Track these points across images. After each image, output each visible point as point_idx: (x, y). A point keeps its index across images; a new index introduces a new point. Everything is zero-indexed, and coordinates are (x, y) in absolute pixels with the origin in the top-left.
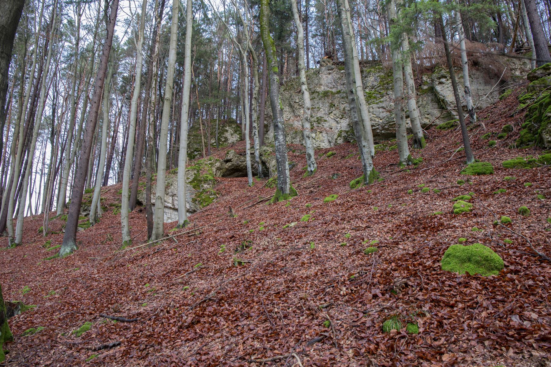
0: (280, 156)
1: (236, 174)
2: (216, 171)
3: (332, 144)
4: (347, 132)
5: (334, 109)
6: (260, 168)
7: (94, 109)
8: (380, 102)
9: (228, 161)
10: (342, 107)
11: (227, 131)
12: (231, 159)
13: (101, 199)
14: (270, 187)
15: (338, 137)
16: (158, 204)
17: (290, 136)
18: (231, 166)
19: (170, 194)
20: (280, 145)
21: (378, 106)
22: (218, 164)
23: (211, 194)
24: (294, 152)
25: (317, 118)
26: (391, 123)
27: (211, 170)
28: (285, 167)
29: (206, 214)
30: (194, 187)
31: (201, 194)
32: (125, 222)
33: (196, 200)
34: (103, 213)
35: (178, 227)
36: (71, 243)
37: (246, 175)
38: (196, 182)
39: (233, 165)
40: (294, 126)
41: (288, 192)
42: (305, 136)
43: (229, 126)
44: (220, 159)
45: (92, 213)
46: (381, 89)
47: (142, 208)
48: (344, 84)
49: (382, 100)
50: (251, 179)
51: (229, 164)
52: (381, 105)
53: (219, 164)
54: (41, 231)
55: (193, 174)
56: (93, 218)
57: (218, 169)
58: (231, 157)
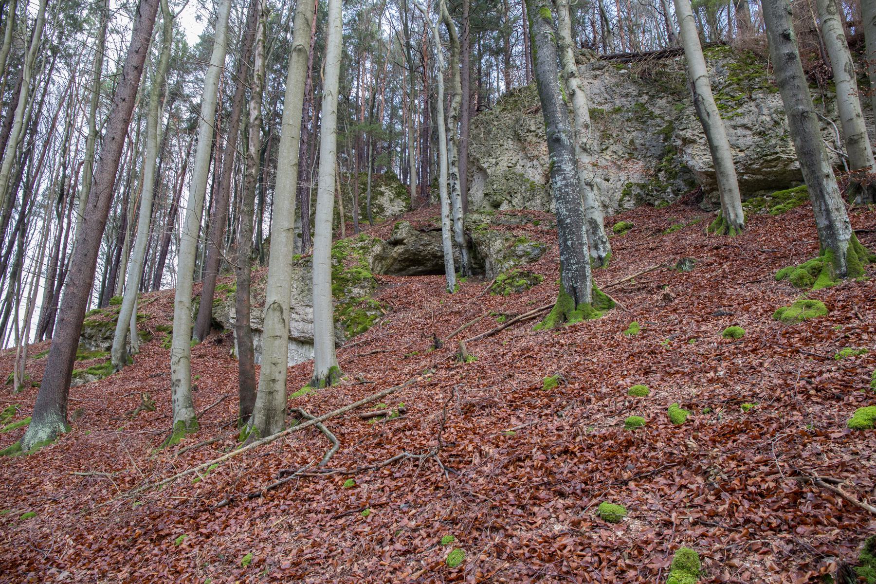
2: (374, 262)
3: (610, 210)
4: (643, 187)
5: (611, 141)
6: (465, 258)
7: (121, 115)
8: (737, 115)
9: (397, 243)
10: (628, 137)
11: (382, 194)
12: (403, 240)
13: (139, 318)
14: (500, 293)
15: (625, 195)
16: (272, 324)
17: (519, 196)
18: (402, 253)
20: (566, 186)
21: (733, 123)
22: (377, 249)
23: (370, 308)
24: (536, 224)
26: (769, 158)
27: (365, 259)
28: (580, 237)
29: (368, 350)
32: (180, 372)
34: (143, 345)
35: (315, 383)
36: (52, 416)
37: (440, 270)
40: (526, 176)
41: (589, 299)
42: (583, 183)
43: (386, 185)
45: (116, 343)
46: (734, 90)
47: (223, 335)
48: (627, 95)
49: (740, 110)
50: (451, 277)
51: (399, 249)
52: (739, 121)
54: (11, 381)
56: (119, 355)
57: (379, 258)
58: (404, 235)
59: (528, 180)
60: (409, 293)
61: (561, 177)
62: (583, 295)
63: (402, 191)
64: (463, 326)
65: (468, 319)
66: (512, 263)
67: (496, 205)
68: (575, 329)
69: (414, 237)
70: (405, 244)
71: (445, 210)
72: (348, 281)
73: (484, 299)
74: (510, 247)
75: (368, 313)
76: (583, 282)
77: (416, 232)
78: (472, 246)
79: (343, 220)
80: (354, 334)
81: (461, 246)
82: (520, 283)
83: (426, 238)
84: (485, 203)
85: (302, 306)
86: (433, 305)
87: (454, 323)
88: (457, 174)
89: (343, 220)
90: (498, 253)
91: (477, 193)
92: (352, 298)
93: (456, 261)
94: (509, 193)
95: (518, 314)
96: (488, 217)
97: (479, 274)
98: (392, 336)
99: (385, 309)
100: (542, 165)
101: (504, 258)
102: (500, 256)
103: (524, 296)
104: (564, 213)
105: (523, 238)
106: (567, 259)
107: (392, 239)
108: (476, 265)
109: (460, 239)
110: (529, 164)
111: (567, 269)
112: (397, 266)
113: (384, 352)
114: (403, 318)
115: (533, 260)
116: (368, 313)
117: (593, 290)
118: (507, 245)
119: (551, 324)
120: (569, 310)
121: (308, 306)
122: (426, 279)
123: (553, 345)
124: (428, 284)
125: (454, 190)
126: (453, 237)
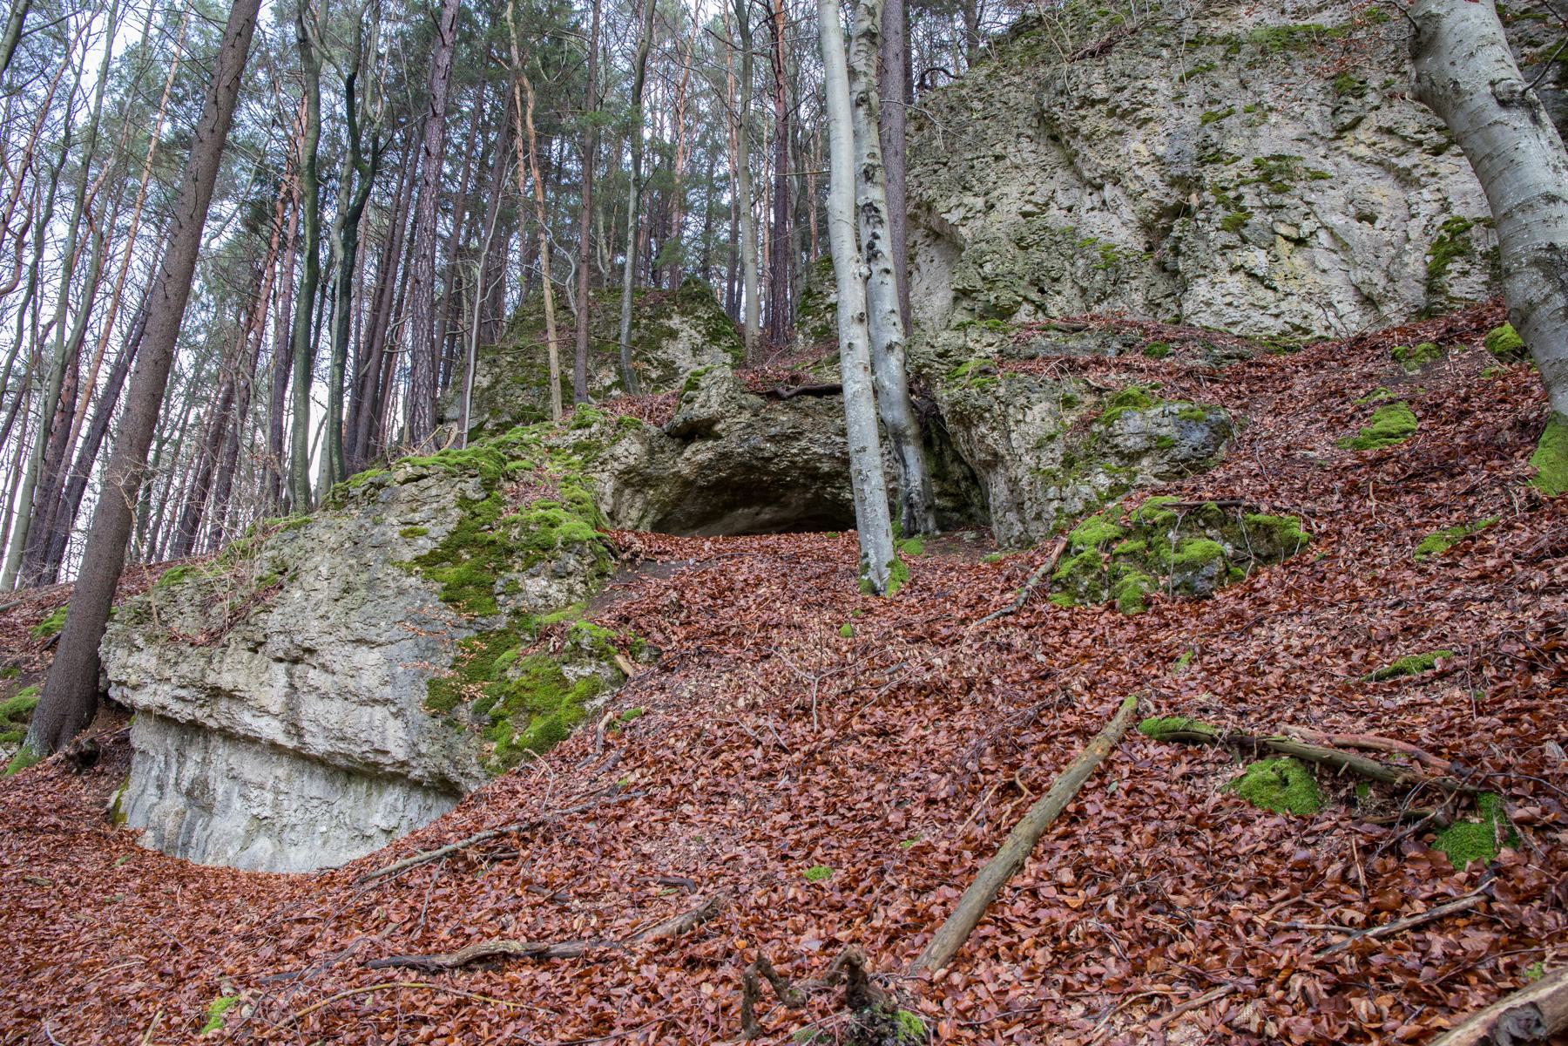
1: (742, 515)
2: (618, 492)
3: (1388, 309)
6: (915, 471)
11: (673, 334)
12: (712, 422)
19: (278, 644)
22: (630, 450)
25: (1258, 165)
31: (497, 649)
37: (837, 517)
39: (724, 456)
40: (1084, 232)
43: (683, 313)
44: (646, 423)
50: (877, 536)
51: (701, 452)
55: (450, 499)
57: (633, 480)
58: (715, 408)
59: (1093, 243)
60: (722, 594)
69: (746, 416)
70: (718, 437)
74: (1085, 424)
75: (569, 672)
77: (753, 399)
83: (784, 419)
85: (344, 642)
88: (881, 207)
90: (1039, 446)
92: (517, 613)
94: (1036, 283)
96: (988, 338)
97: (959, 526)
100: (1134, 197)
101: (1069, 463)
102: (1050, 460)
107: (678, 419)
108: (955, 490)
109: (898, 415)
116: (569, 672)
118: (1071, 418)
121: (360, 641)
122: (786, 544)
124: (794, 559)
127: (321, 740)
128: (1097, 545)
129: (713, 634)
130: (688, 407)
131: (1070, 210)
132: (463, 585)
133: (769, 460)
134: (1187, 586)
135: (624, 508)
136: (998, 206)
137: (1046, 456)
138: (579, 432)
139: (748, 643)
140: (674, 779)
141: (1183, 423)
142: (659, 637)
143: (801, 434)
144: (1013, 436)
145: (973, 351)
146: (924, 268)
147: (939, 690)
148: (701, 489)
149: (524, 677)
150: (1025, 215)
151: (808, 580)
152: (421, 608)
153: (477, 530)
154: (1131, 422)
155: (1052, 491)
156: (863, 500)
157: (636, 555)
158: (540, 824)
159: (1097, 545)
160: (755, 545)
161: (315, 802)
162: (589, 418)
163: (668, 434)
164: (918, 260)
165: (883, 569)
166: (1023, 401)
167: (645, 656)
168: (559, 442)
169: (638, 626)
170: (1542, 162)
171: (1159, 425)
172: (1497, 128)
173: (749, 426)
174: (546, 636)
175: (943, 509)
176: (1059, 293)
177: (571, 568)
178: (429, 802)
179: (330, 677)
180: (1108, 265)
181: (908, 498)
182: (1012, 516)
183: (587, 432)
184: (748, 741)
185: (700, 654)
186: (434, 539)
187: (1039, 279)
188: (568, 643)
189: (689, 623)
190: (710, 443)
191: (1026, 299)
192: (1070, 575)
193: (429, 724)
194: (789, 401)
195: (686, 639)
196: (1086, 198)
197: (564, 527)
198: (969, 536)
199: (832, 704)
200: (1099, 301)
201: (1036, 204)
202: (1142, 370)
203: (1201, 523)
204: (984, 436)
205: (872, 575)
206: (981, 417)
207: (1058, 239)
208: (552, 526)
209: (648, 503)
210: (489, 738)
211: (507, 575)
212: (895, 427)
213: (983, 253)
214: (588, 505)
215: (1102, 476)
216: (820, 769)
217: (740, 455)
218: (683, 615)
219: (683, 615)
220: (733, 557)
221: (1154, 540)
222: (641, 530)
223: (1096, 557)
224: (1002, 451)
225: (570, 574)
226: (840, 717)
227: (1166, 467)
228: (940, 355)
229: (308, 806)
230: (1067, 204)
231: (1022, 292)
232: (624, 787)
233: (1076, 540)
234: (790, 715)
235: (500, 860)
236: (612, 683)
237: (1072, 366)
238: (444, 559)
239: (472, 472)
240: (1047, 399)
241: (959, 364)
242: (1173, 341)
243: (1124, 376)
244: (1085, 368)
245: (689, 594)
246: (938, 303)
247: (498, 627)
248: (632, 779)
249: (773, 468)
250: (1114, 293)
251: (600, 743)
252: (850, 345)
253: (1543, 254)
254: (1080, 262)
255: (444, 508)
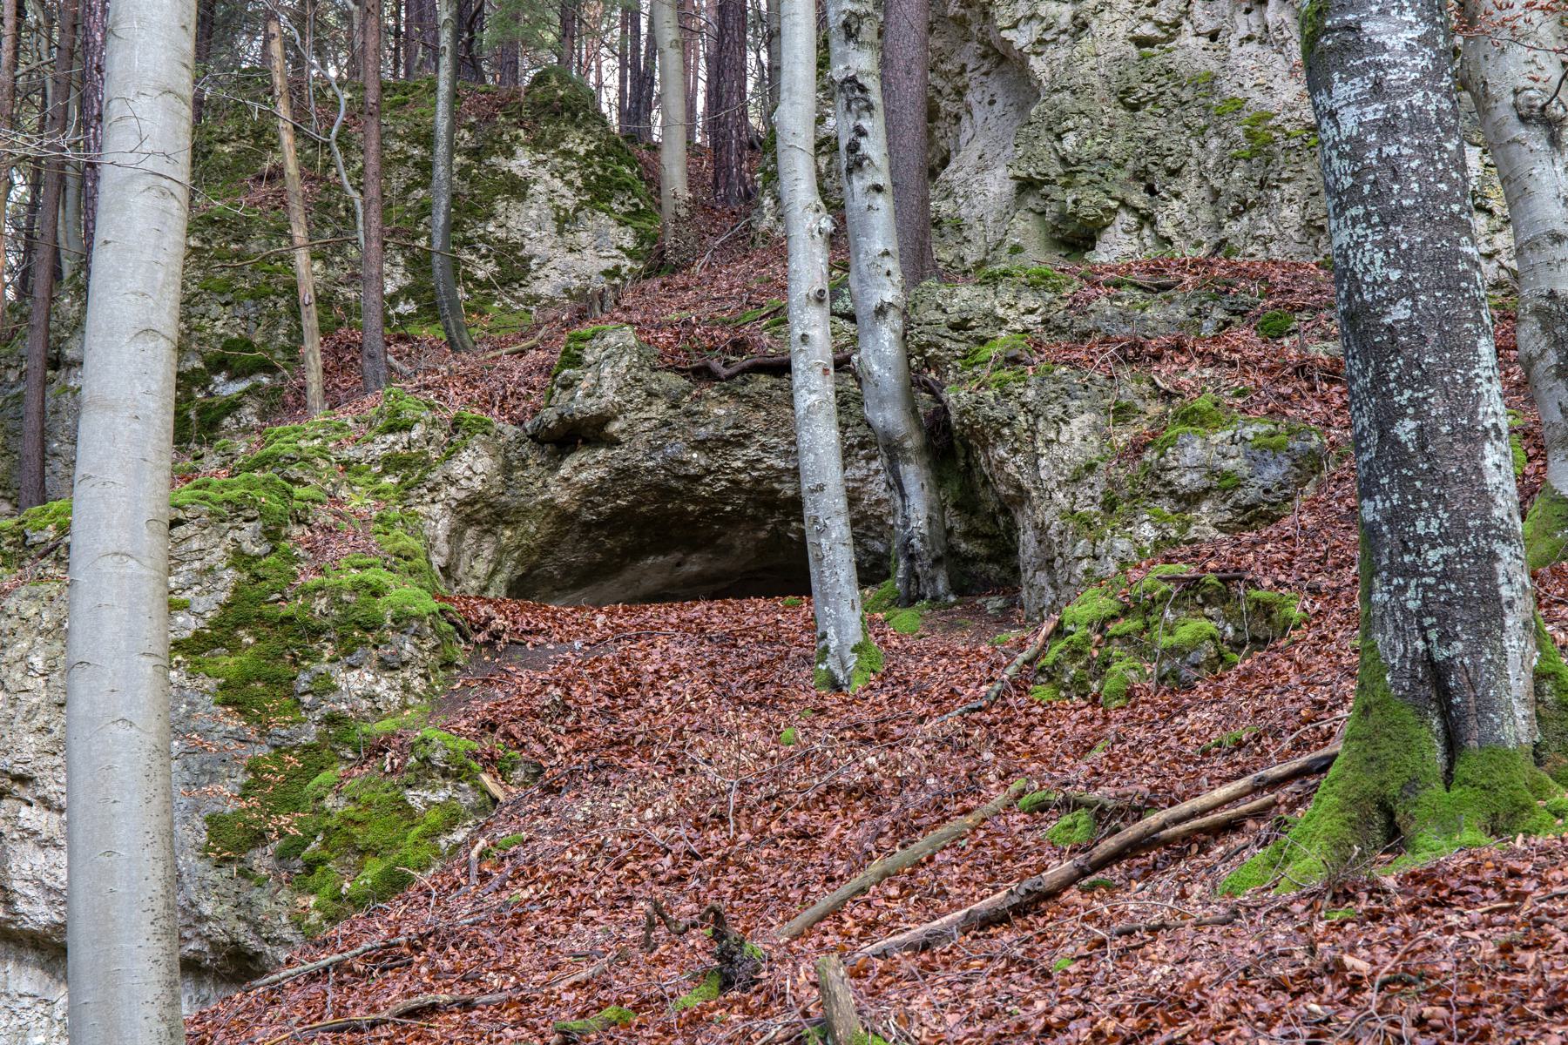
0: (1403, 260)
2: (455, 535)
6: (917, 506)
9: (569, 436)
11: (517, 189)
12: (603, 419)
14: (1080, 685)
20: (1387, 128)
22: (474, 467)
24: (1274, 331)
28: (1465, 399)
29: (394, 995)
30: (234, 697)
33: (259, 838)
37: (787, 572)
38: (254, 645)
39: (624, 474)
40: (1228, 87)
41: (1517, 725)
42: (1504, 111)
43: (536, 144)
50: (840, 606)
51: (586, 468)
53: (484, 464)
57: (480, 514)
58: (610, 396)
59: (1238, 106)
60: (623, 691)
61: (1359, 85)
62: (1486, 706)
63: (619, 172)
64: (876, 866)
65: (905, 831)
66: (1147, 531)
67: (1077, 238)
68: (1432, 892)
69: (659, 408)
70: (613, 442)
71: (808, 266)
72: (316, 633)
73: (1001, 719)
74: (1138, 448)
75: (415, 797)
76: (1482, 636)
78: (950, 447)
79: (310, 320)
80: (340, 907)
81: (893, 450)
82: (1184, 634)
83: (720, 411)
84: (1024, 229)
86: (734, 752)
87: (840, 849)
89: (310, 320)
90: (1076, 479)
91: (982, 184)
92: (332, 720)
93: (865, 524)
94: (1141, 176)
95: (1151, 805)
96: (1028, 300)
97: (988, 586)
98: (519, 921)
99: (503, 773)
101: (1110, 506)
103: (1199, 705)
104: (1378, 272)
105: (1203, 403)
106: (1395, 517)
107: (550, 415)
108: (976, 553)
109: (889, 416)
110: (1244, 24)
111: (1394, 570)
112: (573, 554)
113: (467, 1006)
114: (590, 823)
115: (1254, 516)
116: (415, 797)
117: (1540, 677)
118: (1123, 437)
119: (1310, 863)
120: (1412, 785)
122: (717, 616)
123: (1305, 984)
124: (728, 641)
125: (858, 164)
126: (845, 402)
127: (44, 908)
128: (1090, 625)
129: (612, 744)
130: (566, 395)
131: (1213, 36)
132: (249, 681)
133: (697, 479)
134: (1174, 674)
135: (465, 558)
136: (1094, 24)
137: (1083, 492)
138: (391, 438)
139: (658, 754)
140: (574, 891)
141: (1257, 454)
142: (538, 749)
143: (747, 436)
144: (1043, 462)
145: (1005, 322)
146: (978, 114)
147: (870, 791)
148: (588, 525)
149: (352, 807)
150: (1141, 42)
151: (744, 672)
152: (188, 716)
153: (263, 599)
154: (1188, 451)
155: (1082, 546)
156: (820, 560)
157: (496, 635)
158: (430, 935)
159: (1090, 625)
160: (673, 619)
161: (27, 1002)
162: (408, 415)
163: (533, 437)
164: (970, 97)
165: (847, 654)
166: (1057, 410)
167: (519, 774)
168: (359, 454)
169: (508, 735)
170: (1553, 192)
171: (1224, 456)
172: (1514, 148)
173: (666, 424)
174: (378, 750)
175: (974, 559)
176: (1177, 196)
177: (406, 656)
178: (205, 992)
179: (56, 816)
180: (1255, 152)
181: (907, 545)
182: (1042, 578)
183: (405, 437)
184: (657, 850)
185: (596, 769)
186: (199, 615)
187: (1146, 169)
188: (413, 759)
189: (579, 731)
190: (601, 453)
191: (1123, 203)
192: (1056, 662)
193: (213, 875)
194: (730, 385)
195: (576, 751)
196: (1240, 18)
197: (394, 596)
198: (995, 603)
199: (752, 810)
200: (1236, 215)
201: (1159, 24)
202: (1233, 364)
203: (1199, 599)
204: (1002, 462)
205: (832, 663)
206: (998, 434)
207: (1186, 95)
208: (376, 594)
209: (501, 550)
210: (302, 889)
211: (314, 666)
212: (887, 436)
213: (1063, 116)
214: (420, 561)
215: (1147, 526)
216: (731, 869)
217: (649, 471)
218: (570, 720)
219: (570, 720)
220: (638, 638)
221: (1151, 619)
222: (491, 594)
223: (1087, 640)
224: (1027, 484)
225: (405, 664)
226: (759, 823)
227: (1228, 516)
228: (954, 327)
229: (16, 1007)
230: (1209, 26)
231: (1118, 193)
232: (516, 903)
233: (1067, 618)
234: (705, 825)
235: (392, 968)
236: (475, 811)
237: (1136, 354)
238: (216, 643)
239: (249, 513)
240: (1092, 409)
241: (983, 341)
242: (1302, 309)
243: (1208, 372)
244: (1157, 357)
245: (577, 692)
246: (995, 189)
247: (304, 740)
248: (525, 895)
249: (702, 491)
250: (1260, 203)
251: (474, 872)
252: (804, 338)
253: (1544, 303)
254: (1214, 143)
255: (211, 569)
